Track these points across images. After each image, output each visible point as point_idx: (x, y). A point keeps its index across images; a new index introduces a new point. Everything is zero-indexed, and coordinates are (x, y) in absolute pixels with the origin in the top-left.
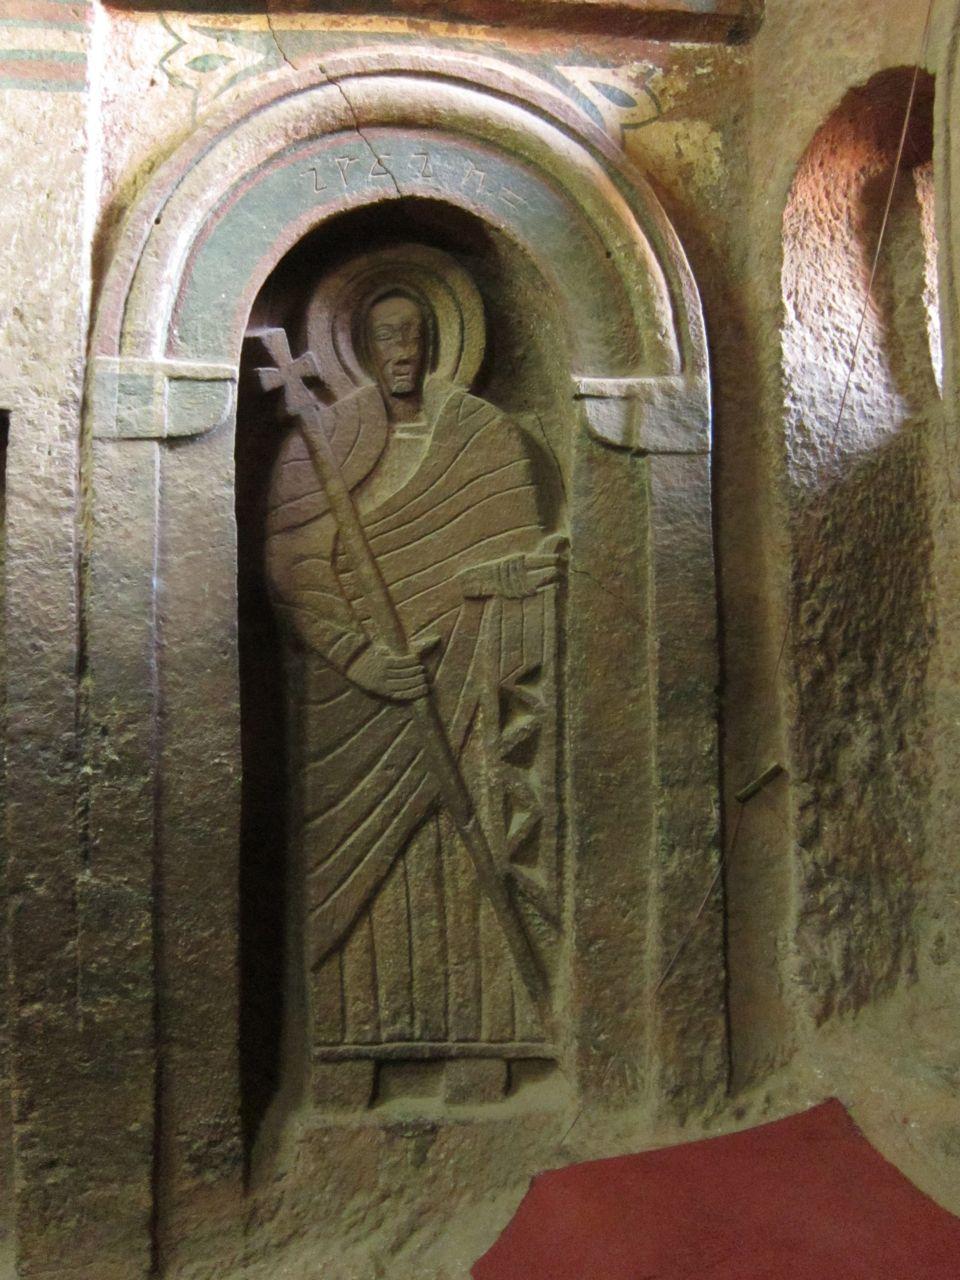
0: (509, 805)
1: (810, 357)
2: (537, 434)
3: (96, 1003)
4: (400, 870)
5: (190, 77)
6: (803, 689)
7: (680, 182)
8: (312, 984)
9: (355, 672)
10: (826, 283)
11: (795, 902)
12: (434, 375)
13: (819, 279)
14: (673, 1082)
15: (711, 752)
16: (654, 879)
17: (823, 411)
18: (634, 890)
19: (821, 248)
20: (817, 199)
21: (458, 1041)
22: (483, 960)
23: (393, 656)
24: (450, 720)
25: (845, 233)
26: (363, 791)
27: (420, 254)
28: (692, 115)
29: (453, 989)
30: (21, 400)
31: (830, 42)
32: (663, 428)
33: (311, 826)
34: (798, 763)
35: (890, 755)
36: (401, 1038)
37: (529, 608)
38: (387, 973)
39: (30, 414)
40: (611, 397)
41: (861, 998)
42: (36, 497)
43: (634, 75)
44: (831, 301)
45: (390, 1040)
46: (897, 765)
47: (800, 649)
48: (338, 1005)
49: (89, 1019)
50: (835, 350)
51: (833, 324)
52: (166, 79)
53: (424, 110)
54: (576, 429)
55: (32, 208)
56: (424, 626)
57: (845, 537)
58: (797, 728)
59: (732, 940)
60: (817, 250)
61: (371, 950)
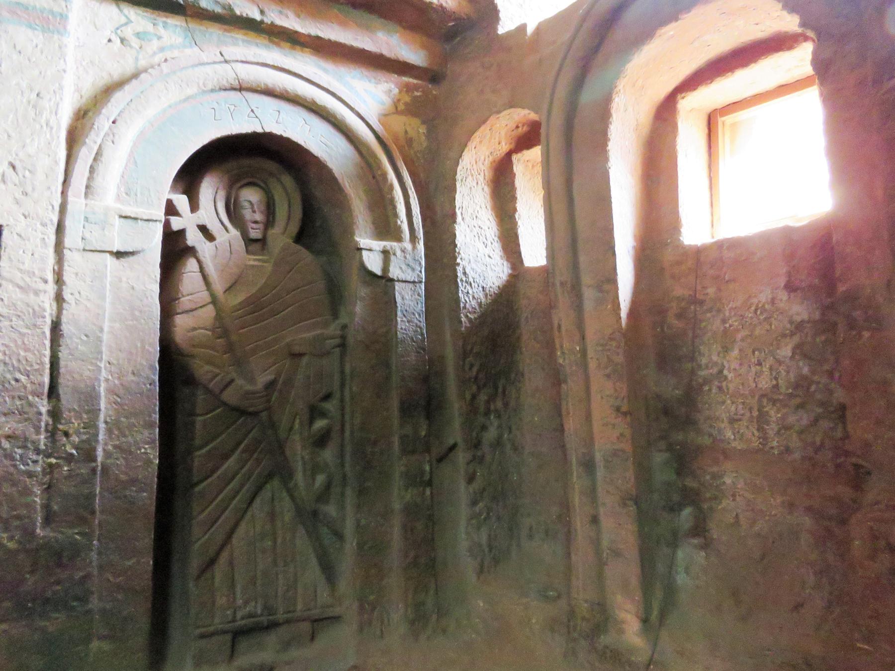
0: (315, 469)
1: (468, 239)
4: (249, 514)
5: (135, 42)
6: (467, 403)
10: (474, 204)
12: (273, 231)
13: (472, 203)
16: (397, 506)
17: (474, 266)
25: (482, 182)
27: (271, 165)
29: (281, 582)
30: (11, 220)
32: (401, 268)
35: (506, 436)
37: (324, 362)
39: (18, 229)
40: (375, 251)
41: (496, 561)
42: (22, 284)
45: (242, 618)
46: (509, 440)
47: (463, 382)
50: (479, 237)
52: (119, 41)
53: (280, 88)
55: (24, 100)
60: (471, 188)
61: (231, 564)
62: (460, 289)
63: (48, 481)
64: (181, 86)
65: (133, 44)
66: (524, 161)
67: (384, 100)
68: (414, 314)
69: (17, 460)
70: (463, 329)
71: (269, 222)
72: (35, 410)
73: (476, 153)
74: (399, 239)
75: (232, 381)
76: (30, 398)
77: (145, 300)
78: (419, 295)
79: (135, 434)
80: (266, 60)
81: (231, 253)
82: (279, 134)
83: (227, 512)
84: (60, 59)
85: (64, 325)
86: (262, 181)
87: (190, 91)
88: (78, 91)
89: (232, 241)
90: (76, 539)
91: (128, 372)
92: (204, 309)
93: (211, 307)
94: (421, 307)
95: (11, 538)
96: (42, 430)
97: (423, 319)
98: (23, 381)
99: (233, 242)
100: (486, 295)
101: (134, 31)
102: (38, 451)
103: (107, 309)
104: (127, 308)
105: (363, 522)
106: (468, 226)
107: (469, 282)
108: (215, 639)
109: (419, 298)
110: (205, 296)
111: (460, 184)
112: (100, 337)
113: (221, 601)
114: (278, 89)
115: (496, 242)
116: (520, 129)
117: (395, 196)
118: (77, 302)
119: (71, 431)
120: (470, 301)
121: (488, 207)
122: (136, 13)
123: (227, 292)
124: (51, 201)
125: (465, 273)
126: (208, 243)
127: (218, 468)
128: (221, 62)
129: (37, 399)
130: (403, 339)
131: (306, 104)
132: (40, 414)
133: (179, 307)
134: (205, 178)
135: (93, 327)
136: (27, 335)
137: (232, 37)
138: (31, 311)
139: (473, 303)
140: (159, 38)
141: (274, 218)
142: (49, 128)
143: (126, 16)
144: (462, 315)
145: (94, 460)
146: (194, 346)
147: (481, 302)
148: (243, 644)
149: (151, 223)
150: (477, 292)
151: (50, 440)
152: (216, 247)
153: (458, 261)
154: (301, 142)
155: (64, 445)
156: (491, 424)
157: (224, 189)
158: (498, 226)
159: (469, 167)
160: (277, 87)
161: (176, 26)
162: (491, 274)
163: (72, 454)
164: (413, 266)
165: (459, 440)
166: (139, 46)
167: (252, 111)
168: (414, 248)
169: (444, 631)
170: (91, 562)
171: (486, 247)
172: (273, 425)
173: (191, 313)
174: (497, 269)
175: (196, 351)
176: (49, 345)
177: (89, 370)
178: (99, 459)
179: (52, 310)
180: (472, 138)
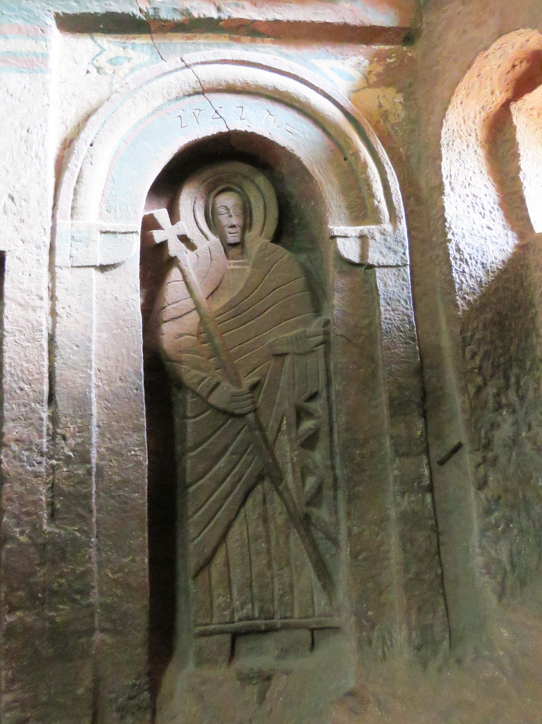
2: (309, 264)
3: (57, 610)
4: (242, 515)
5: (109, 69)
7: (382, 121)
8: (192, 587)
9: (213, 400)
10: (466, 170)
11: (476, 525)
12: (251, 234)
14: (417, 642)
15: (421, 436)
16: (393, 513)
17: (469, 240)
18: (382, 521)
19: (462, 152)
20: (459, 124)
21: (281, 618)
22: (293, 567)
23: (234, 390)
24: (268, 425)
25: (474, 144)
26: (219, 468)
28: (388, 85)
29: (277, 585)
30: (12, 246)
31: (465, 32)
32: (381, 252)
33: (191, 489)
34: (472, 441)
35: (524, 434)
36: (248, 618)
37: (309, 360)
38: (237, 575)
39: (18, 253)
42: (22, 302)
43: (353, 64)
44: (470, 180)
45: (240, 620)
48: (209, 599)
49: (52, 620)
51: (471, 193)
52: (96, 70)
54: (331, 254)
55: (18, 137)
56: (251, 372)
57: (488, 310)
58: (470, 420)
59: (442, 549)
60: (460, 152)
61: (227, 564)
62: (454, 269)
63: (51, 482)
64: (147, 99)
65: (107, 71)
66: (527, 109)
67: (354, 76)
68: (399, 301)
69: (24, 462)
70: (460, 313)
71: (246, 226)
72: (37, 416)
73: (463, 111)
74: (378, 221)
75: (217, 384)
76: (33, 404)
77: (128, 309)
78: (404, 279)
79: (125, 437)
80: (225, 57)
81: (212, 260)
82: (244, 130)
83: (220, 513)
84: (44, 95)
85: (57, 337)
86: (237, 186)
87: (156, 103)
88: (64, 123)
89: (212, 247)
90: (76, 536)
91: (116, 379)
92: (189, 316)
93: (195, 313)
94: (407, 293)
95: (22, 533)
96: (44, 434)
97: (410, 306)
98: (26, 389)
99: (212, 248)
100: (487, 272)
101: (107, 58)
102: (42, 454)
103: (94, 320)
104: (112, 318)
105: (355, 529)
106: (460, 196)
107: (464, 260)
108: (215, 638)
109: (405, 283)
110: (189, 303)
111: (446, 149)
112: (89, 347)
113: (219, 601)
114: (239, 84)
115: (496, 210)
116: (517, 68)
117: (370, 174)
118: (68, 315)
119: (68, 435)
120: (467, 281)
121: (483, 172)
122: (108, 41)
123: (211, 298)
124: (43, 225)
125: (458, 250)
126: (189, 252)
127: (210, 470)
128: (182, 68)
129: (38, 405)
130: (388, 329)
131: (268, 94)
132: (41, 419)
133: (165, 315)
134: (183, 190)
135: (82, 337)
136: (28, 348)
137: (194, 43)
138: (30, 326)
139: (471, 283)
140: (129, 59)
141: (251, 221)
142: (38, 159)
143: (99, 46)
144: (458, 297)
145: (89, 461)
146: (181, 352)
147: (481, 281)
148: (242, 645)
149: (128, 235)
150: (475, 270)
151: (51, 442)
152: (197, 255)
153: (450, 236)
154: (266, 135)
155: (63, 448)
156: (504, 420)
157: (202, 198)
158: (497, 191)
159: (456, 127)
160: (237, 81)
161: (144, 44)
162: (492, 247)
163: (69, 457)
164: (396, 248)
165: (465, 440)
166: (113, 71)
167: (216, 112)
168: (395, 228)
169: (459, 661)
170: (90, 558)
171: (484, 217)
172: (261, 429)
173: (176, 320)
174: (499, 241)
175: (184, 356)
176: (48, 356)
177: (81, 377)
178: (94, 461)
179: (48, 324)
180: (456, 91)
